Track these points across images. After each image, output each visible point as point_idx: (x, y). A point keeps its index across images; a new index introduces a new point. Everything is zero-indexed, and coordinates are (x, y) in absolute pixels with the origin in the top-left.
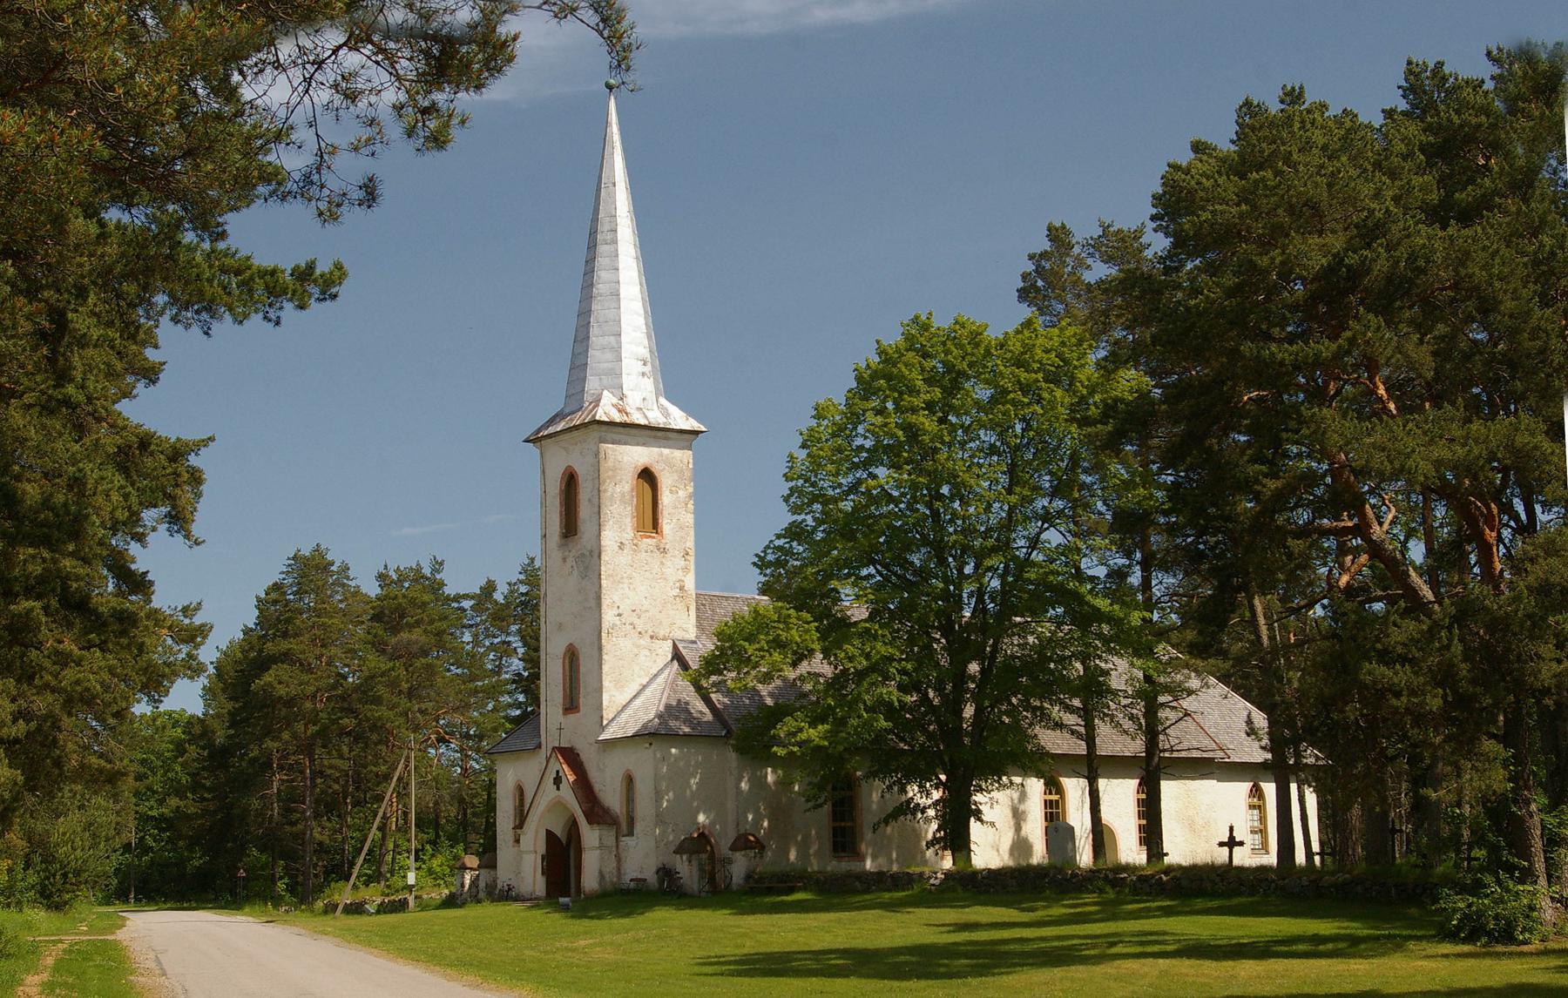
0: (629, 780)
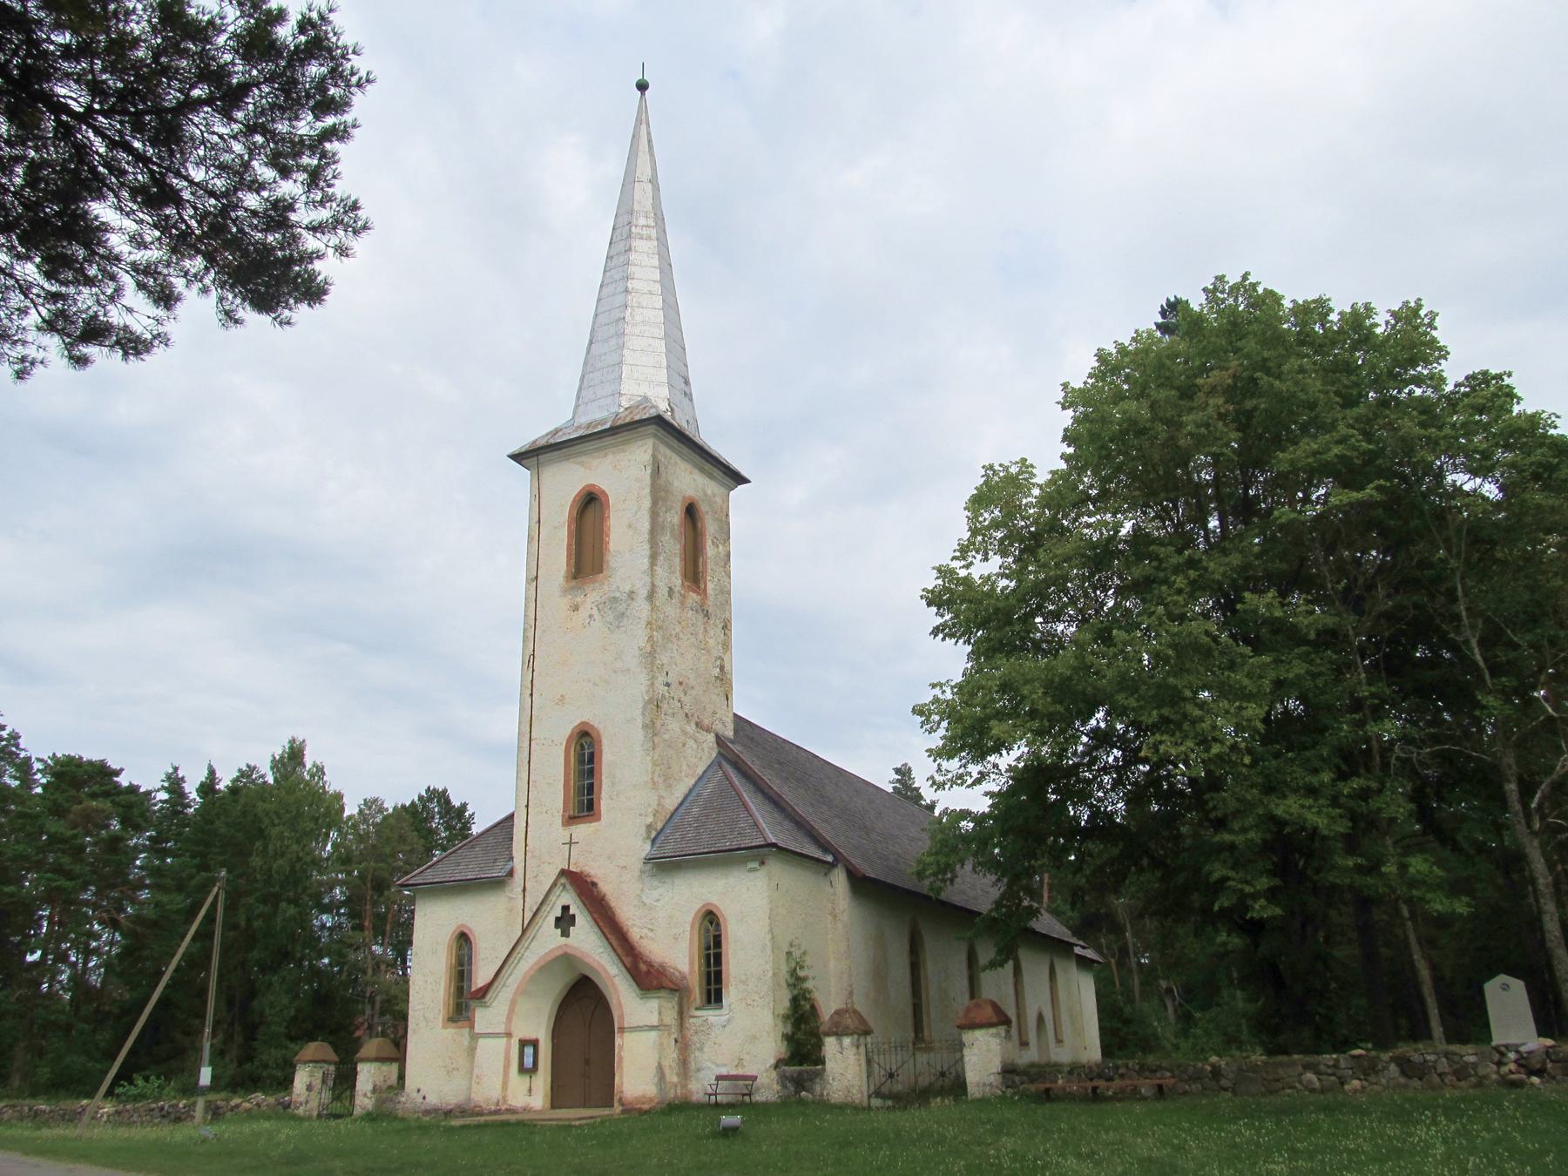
0: (711, 921)
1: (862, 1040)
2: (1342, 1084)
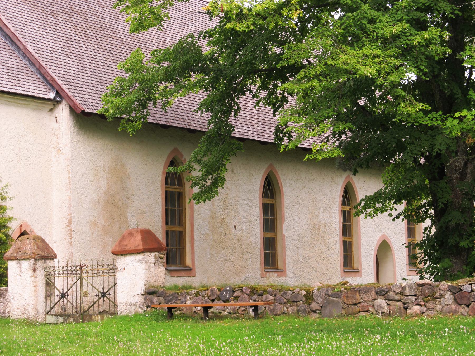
1: (39, 263)
2: (406, 309)
